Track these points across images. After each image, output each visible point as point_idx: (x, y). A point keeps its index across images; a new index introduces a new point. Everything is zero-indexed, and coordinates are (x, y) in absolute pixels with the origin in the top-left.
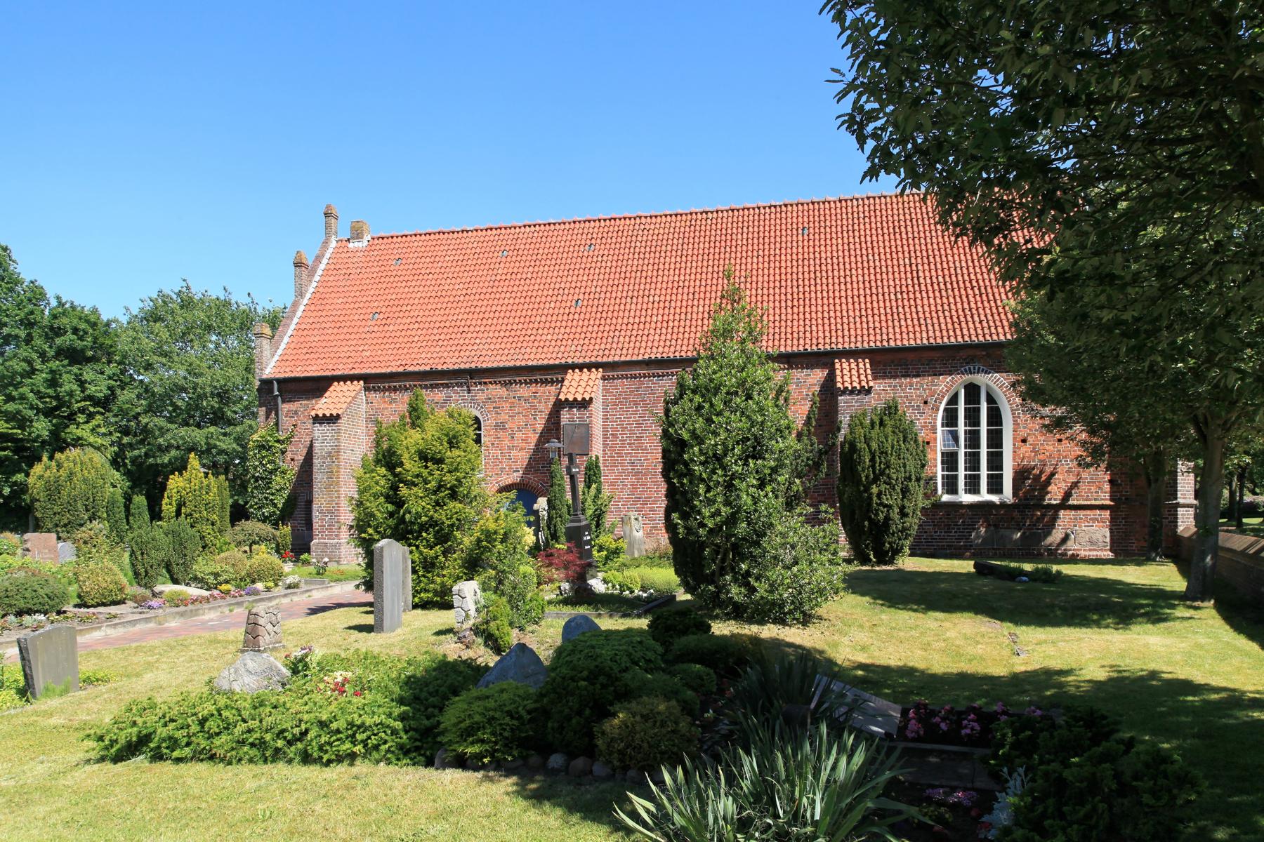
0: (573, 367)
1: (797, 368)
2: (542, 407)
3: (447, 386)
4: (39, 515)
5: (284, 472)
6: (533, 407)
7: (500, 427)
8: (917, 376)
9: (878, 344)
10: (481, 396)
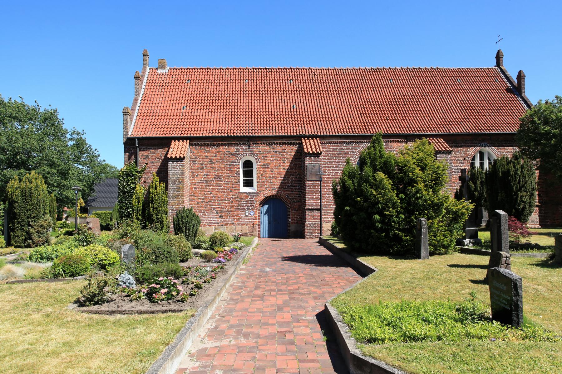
0: (175, 139)
1: (410, 142)
2: (288, 156)
3: (237, 144)
4: (17, 211)
6: (283, 156)
7: (266, 166)
8: (461, 147)
9: (244, 134)
10: (256, 150)
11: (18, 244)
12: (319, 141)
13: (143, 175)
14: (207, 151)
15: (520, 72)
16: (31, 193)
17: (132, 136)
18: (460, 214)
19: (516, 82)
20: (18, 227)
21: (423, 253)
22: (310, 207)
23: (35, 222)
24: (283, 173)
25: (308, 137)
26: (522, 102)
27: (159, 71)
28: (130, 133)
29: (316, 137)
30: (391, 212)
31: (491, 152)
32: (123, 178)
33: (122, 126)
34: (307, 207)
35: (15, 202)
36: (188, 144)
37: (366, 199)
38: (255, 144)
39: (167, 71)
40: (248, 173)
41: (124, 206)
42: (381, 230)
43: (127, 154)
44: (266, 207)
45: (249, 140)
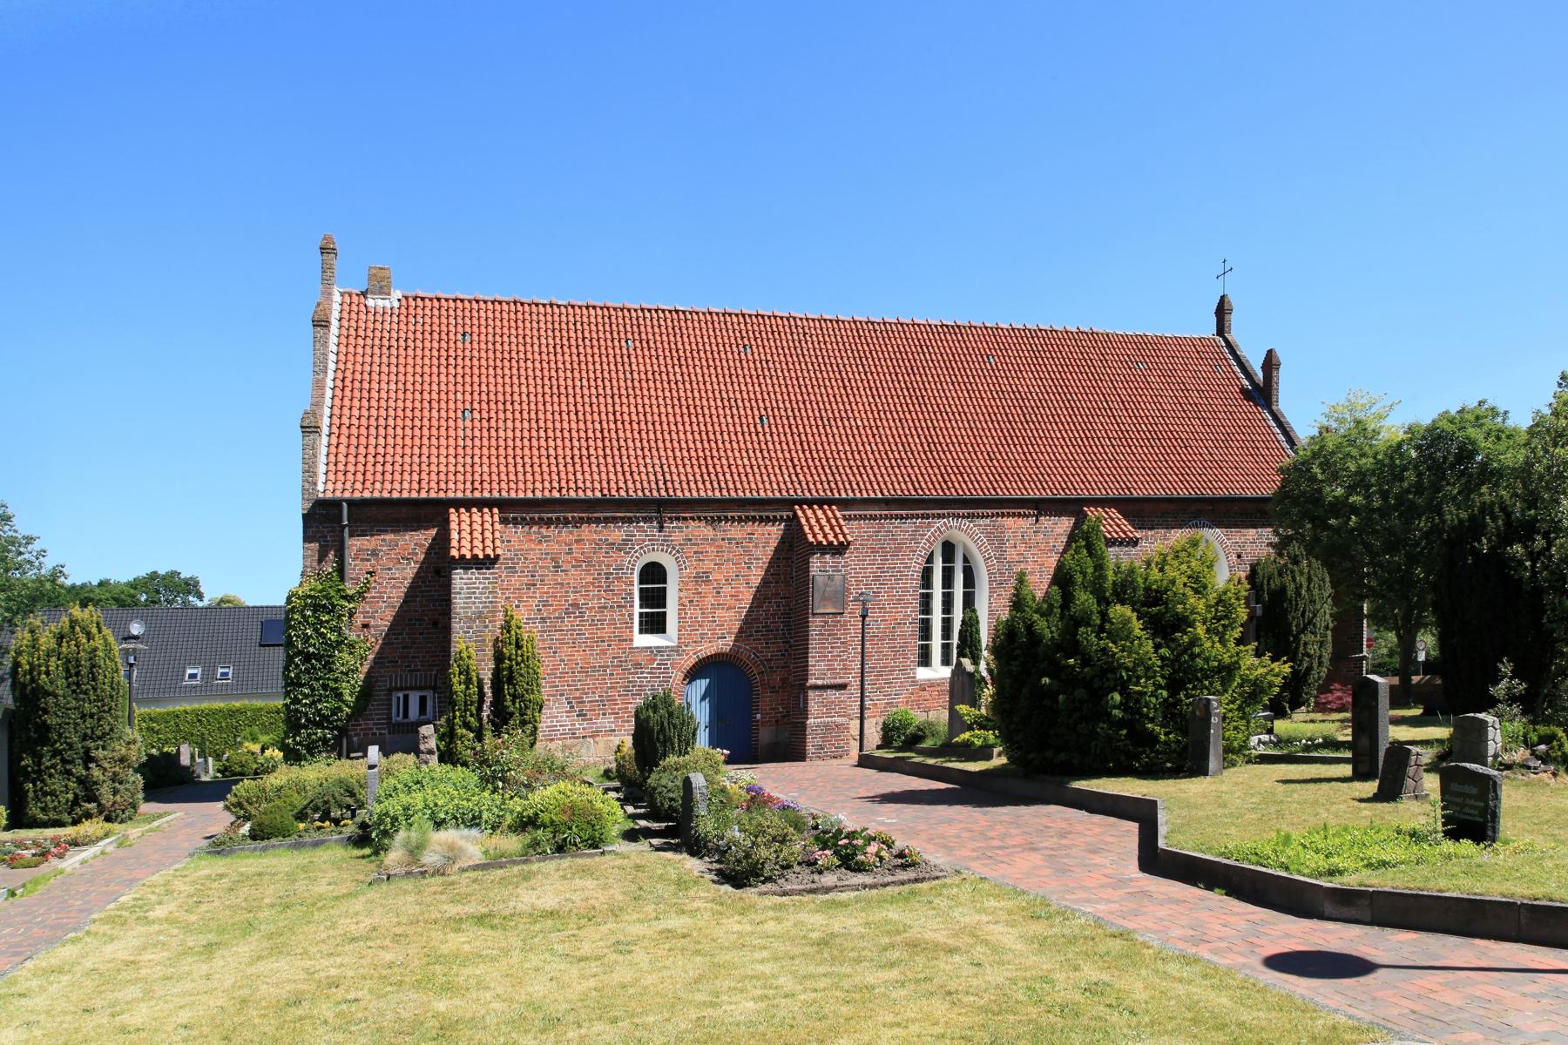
2: (758, 553)
3: (630, 521)
4: (51, 720)
5: (351, 646)
6: (747, 552)
7: (702, 578)
8: (1152, 528)
10: (678, 537)
11: (53, 815)
12: (838, 514)
13: (361, 607)
14: (547, 539)
15: (1270, 352)
16: (93, 666)
17: (329, 495)
18: (1265, 685)
19: (1260, 375)
20: (53, 766)
21: (1213, 764)
22: (820, 682)
23: (104, 748)
24: (747, 597)
25: (810, 503)
26: (1272, 423)
27: (370, 303)
28: (320, 487)
29: (830, 502)
30: (1143, 686)
31: (1211, 539)
32: (304, 616)
33: (298, 466)
34: (812, 681)
35: (48, 694)
36: (496, 518)
37: (1086, 661)
38: (678, 519)
39: (396, 304)
40: (654, 600)
41: (306, 696)
42: (1121, 724)
43: (315, 546)
44: (701, 685)
45: (661, 509)
